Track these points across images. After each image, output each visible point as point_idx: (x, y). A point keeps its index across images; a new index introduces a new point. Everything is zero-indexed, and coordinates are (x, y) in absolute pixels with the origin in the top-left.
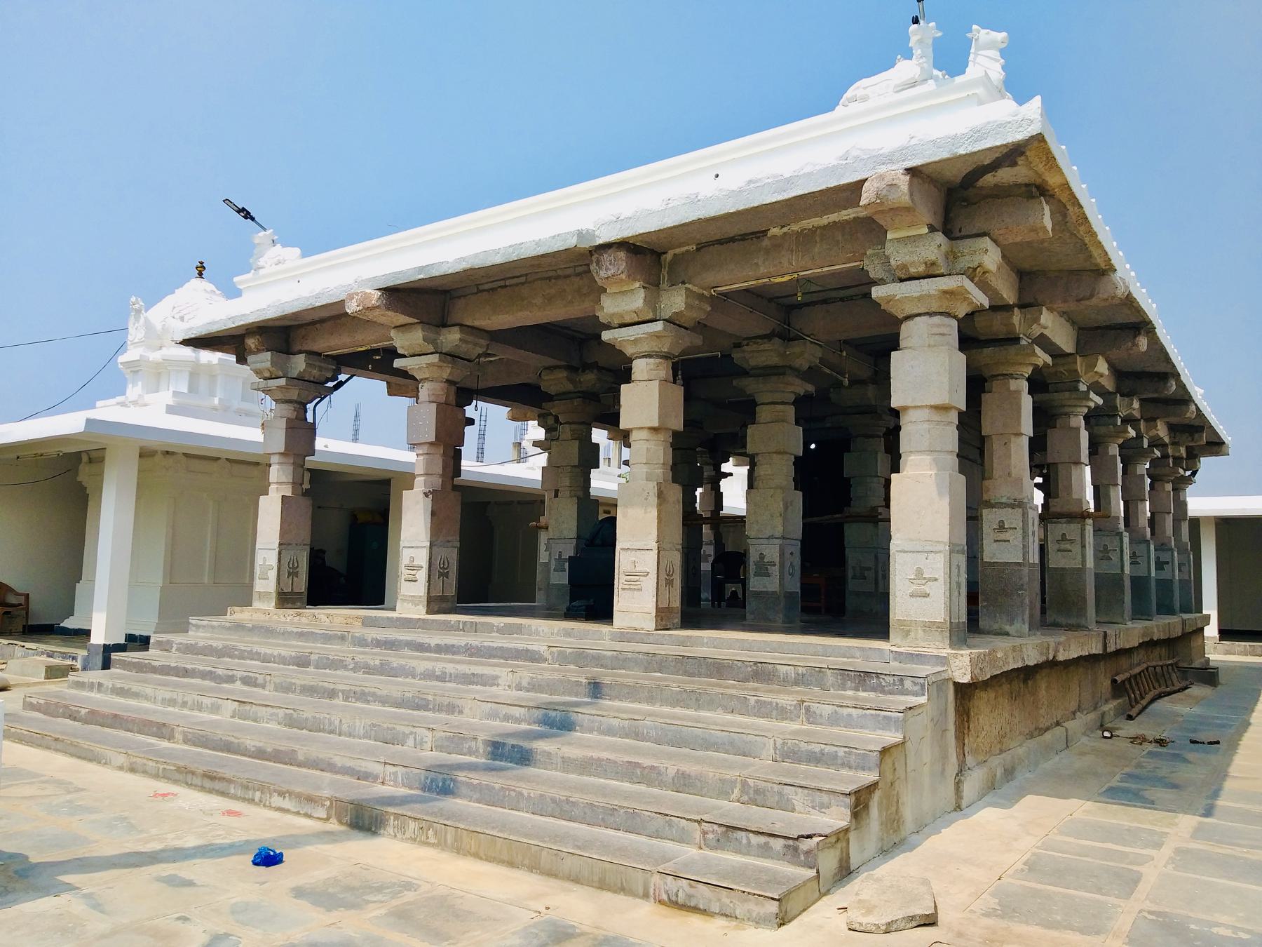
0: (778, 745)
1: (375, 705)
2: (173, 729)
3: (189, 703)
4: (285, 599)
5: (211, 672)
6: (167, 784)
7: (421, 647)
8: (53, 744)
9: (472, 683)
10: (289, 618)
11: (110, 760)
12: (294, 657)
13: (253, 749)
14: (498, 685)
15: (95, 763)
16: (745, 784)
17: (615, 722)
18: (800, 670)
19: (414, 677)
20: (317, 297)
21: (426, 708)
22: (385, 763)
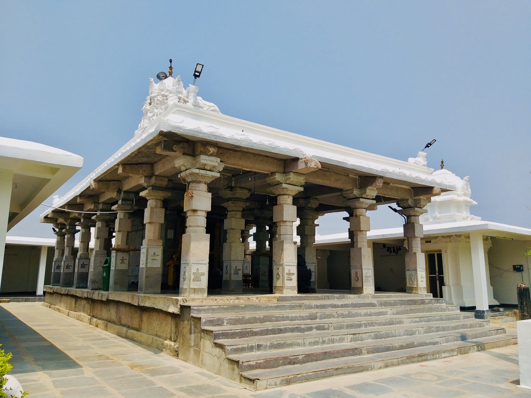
1: (377, 327)
2: (361, 350)
3: (327, 341)
5: (297, 328)
6: (404, 366)
7: (335, 306)
8: (335, 372)
9: (380, 315)
10: (231, 301)
11: (374, 366)
12: (308, 316)
13: (398, 346)
14: (388, 314)
15: (364, 371)
18: (429, 300)
19: (361, 316)
21: (393, 324)
22: (440, 337)
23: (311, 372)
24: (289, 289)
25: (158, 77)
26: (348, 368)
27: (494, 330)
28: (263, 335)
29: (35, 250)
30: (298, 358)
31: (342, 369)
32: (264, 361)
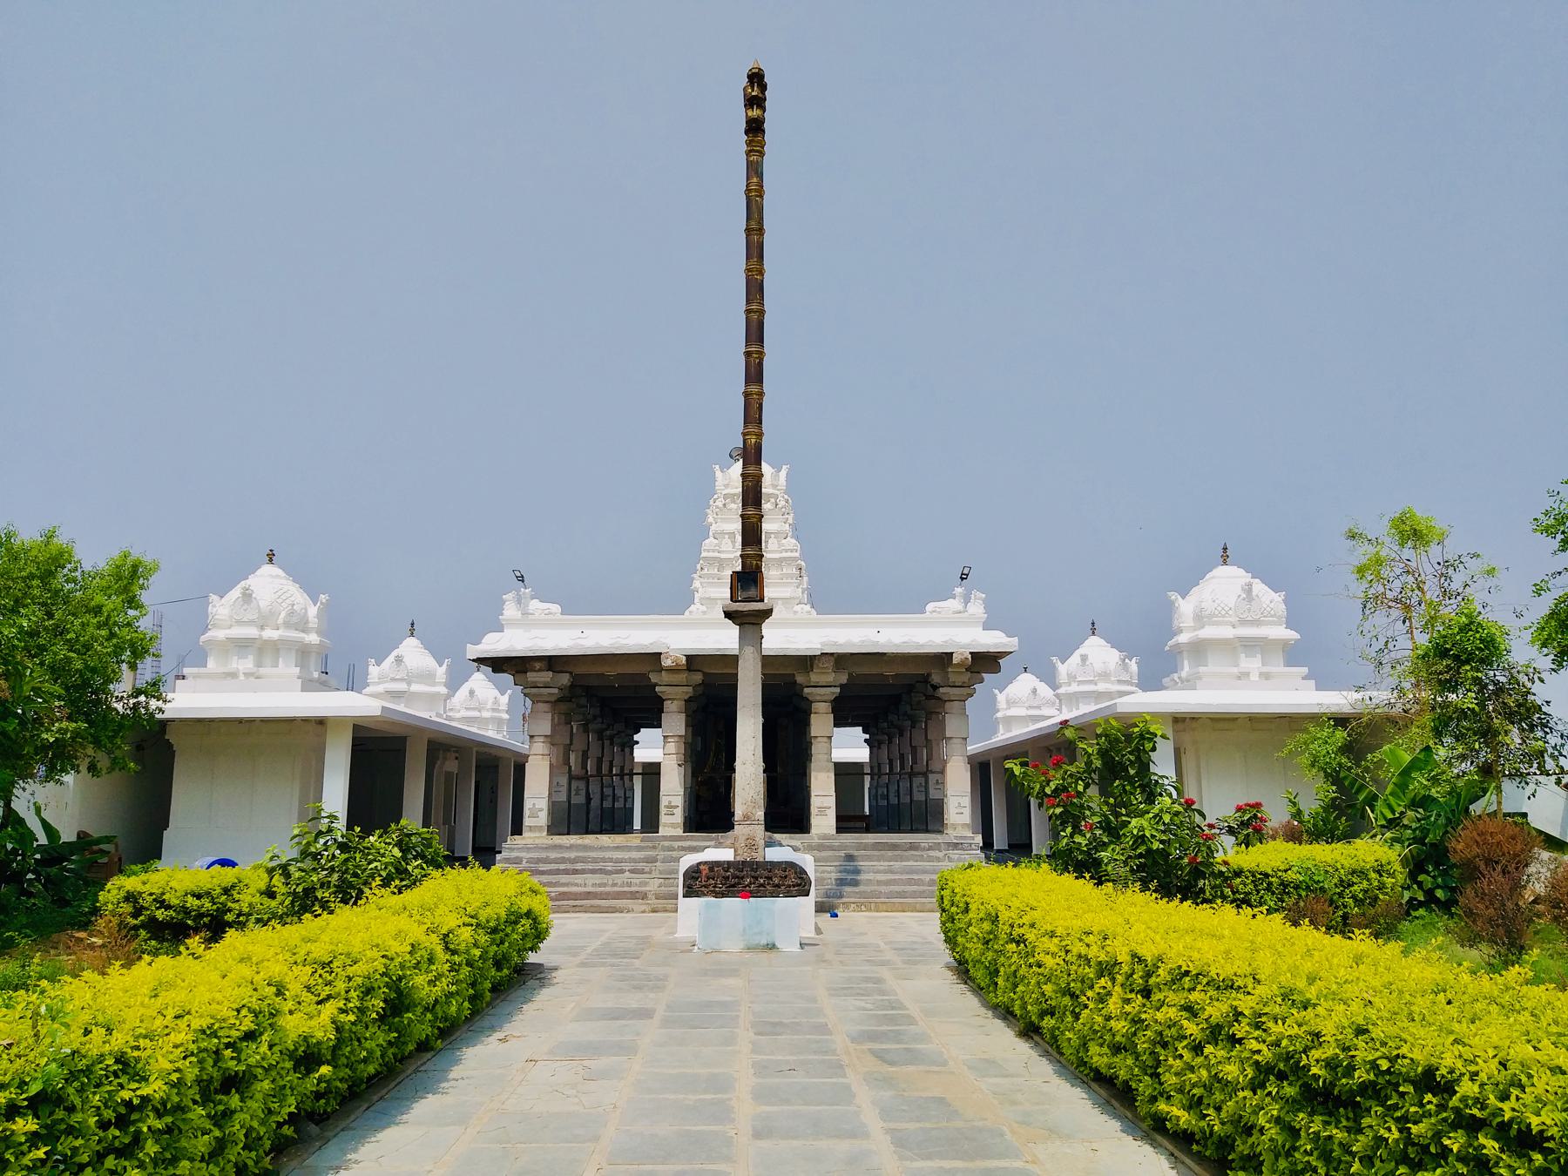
2: (646, 894)
4: (553, 829)
20: (617, 648)
24: (669, 827)
25: (731, 456)
29: (859, 765)
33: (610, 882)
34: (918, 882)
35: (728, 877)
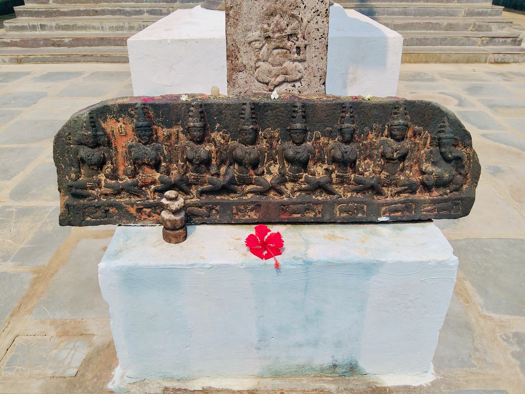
0: (466, 11)
5: (120, 10)
8: (83, 58)
16: (475, 24)
17: (396, 10)
23: (49, 55)
26: (102, 56)
27: (481, 37)
28: (74, 16)
30: (64, 41)
31: (93, 57)
32: (20, 40)
33: (127, 25)
34: (435, 27)
35: (207, 162)
